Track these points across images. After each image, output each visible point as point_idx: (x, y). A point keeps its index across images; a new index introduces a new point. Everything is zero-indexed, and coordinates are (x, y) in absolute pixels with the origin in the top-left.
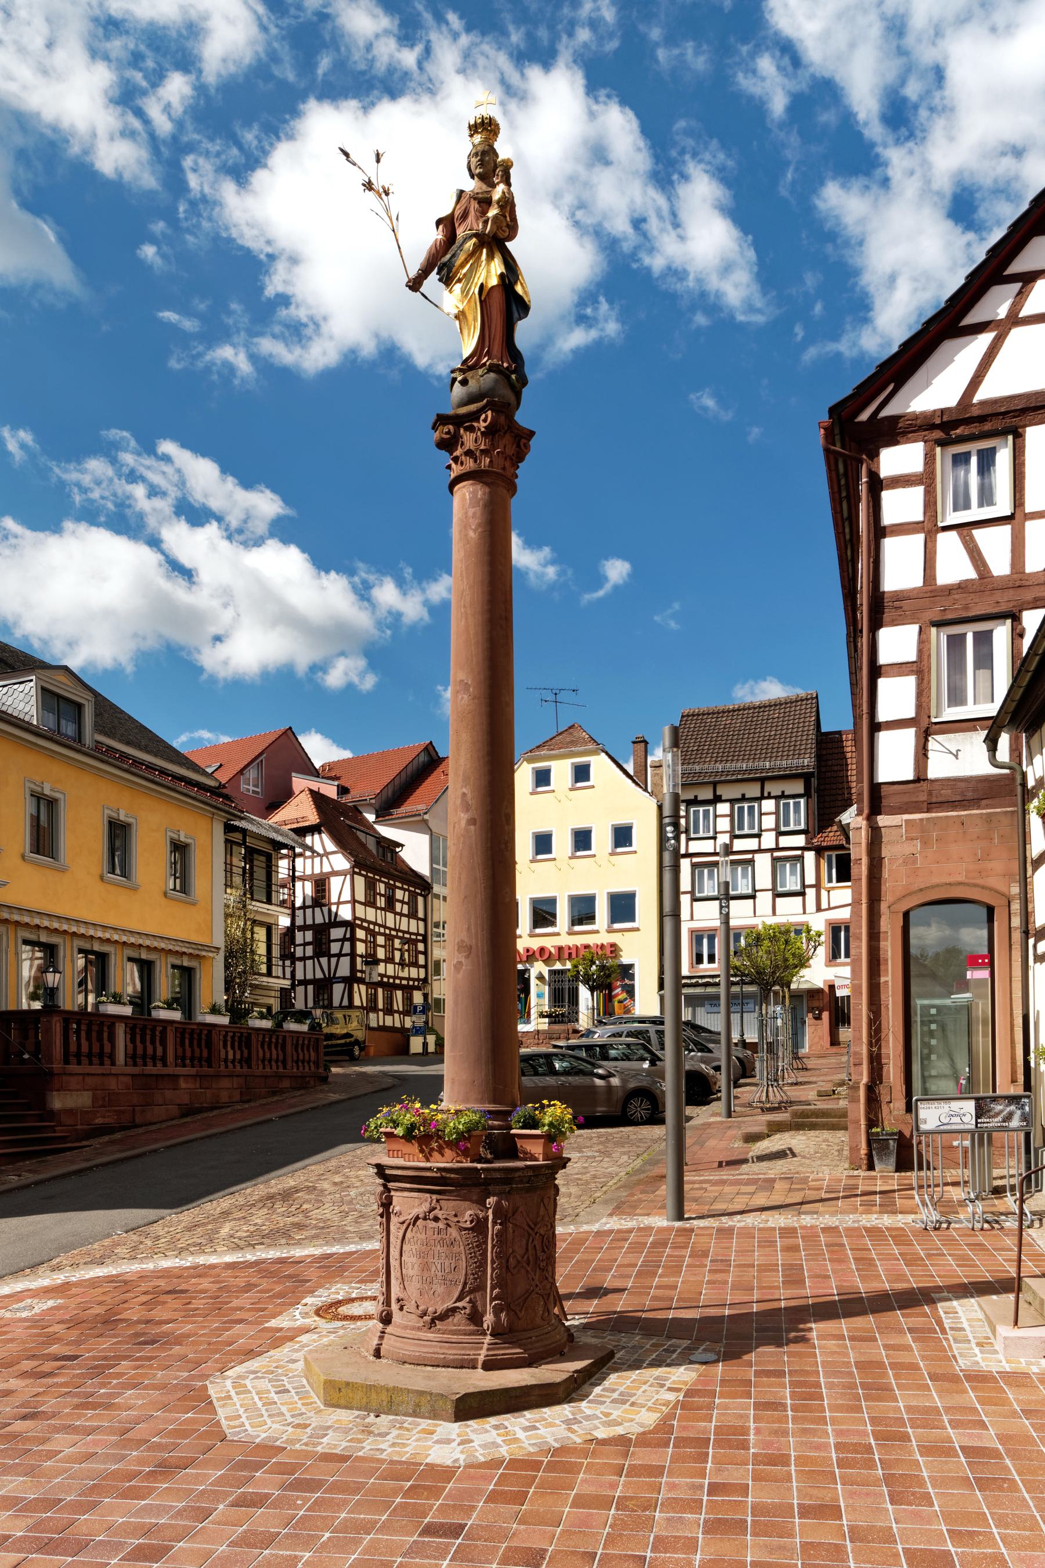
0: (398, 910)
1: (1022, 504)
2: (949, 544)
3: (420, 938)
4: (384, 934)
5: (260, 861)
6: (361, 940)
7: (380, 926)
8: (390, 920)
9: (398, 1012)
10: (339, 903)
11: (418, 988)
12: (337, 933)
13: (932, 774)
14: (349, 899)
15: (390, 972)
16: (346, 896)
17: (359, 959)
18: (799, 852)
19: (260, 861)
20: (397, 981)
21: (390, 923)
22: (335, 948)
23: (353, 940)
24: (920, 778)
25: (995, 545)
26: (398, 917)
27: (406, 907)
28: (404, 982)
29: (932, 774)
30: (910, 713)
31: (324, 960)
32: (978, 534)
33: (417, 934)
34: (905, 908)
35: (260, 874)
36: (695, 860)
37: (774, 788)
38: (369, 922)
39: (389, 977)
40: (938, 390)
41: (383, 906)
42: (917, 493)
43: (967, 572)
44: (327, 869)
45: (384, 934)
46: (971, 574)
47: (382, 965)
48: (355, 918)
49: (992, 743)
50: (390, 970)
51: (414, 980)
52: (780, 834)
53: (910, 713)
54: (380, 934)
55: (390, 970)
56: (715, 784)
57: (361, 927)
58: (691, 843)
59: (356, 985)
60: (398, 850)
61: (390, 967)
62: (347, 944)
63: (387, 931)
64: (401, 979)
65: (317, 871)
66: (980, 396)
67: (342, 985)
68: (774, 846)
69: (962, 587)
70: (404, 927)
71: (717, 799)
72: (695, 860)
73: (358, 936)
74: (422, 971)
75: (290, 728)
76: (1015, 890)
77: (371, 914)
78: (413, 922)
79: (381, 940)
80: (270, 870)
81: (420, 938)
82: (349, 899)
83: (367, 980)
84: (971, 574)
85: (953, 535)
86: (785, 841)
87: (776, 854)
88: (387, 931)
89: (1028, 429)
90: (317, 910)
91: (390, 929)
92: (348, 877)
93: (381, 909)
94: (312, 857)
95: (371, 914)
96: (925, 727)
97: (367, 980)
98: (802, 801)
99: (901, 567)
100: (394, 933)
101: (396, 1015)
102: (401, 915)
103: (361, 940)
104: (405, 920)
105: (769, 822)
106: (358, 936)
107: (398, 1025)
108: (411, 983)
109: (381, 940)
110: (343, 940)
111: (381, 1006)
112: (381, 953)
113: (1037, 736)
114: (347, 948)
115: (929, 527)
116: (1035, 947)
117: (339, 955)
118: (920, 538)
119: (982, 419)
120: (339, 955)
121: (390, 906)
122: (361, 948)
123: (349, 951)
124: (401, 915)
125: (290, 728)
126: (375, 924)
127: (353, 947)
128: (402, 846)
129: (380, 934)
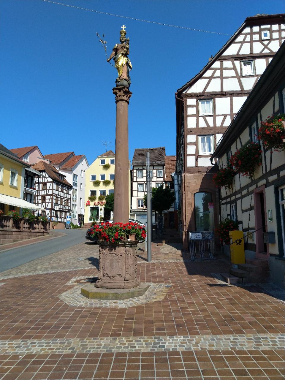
0: (64, 192)
1: (233, 112)
2: (201, 119)
3: (69, 199)
4: (60, 198)
5: (30, 178)
6: (54, 199)
7: (59, 196)
8: (62, 194)
9: (63, 218)
10: (49, 190)
11: (69, 212)
12: (48, 197)
13: (199, 165)
14: (52, 189)
15: (61, 208)
16: (51, 188)
17: (54, 204)
18: (162, 182)
19: (30, 178)
20: (63, 210)
21: (62, 195)
22: (47, 201)
23: (52, 199)
24: (196, 166)
25: (210, 120)
26: (64, 194)
27: (66, 191)
28: (65, 210)
29: (199, 165)
30: (194, 153)
31: (44, 204)
32: (207, 118)
33: (69, 198)
34: (194, 193)
35: (29, 181)
36: (138, 183)
37: (156, 168)
38: (57, 195)
39: (61, 209)
40: (198, 87)
41: (60, 191)
42: (195, 109)
43: (205, 125)
44: (46, 181)
45: (60, 198)
46: (206, 126)
47: (60, 206)
48: (53, 193)
49: (211, 160)
50: (61, 207)
51: (67, 210)
52: (158, 178)
53: (194, 153)
54: (59, 198)
55: (61, 207)
56: (143, 166)
57: (55, 196)
58: (137, 179)
59: (52, 211)
60: (64, 177)
61: (61, 206)
62: (51, 200)
63: (61, 197)
64: (64, 209)
65: (44, 181)
66: (207, 91)
67: (49, 210)
68: (156, 180)
69: (204, 128)
70: (65, 196)
71: (143, 169)
72: (138, 183)
73: (54, 198)
74: (69, 207)
75: (37, 146)
76: (217, 190)
77: (57, 193)
78: (68, 195)
79: (59, 199)
80: (32, 180)
81: (69, 199)
82: (52, 189)
83: (56, 209)
84: (206, 126)
85: (202, 118)
86: (159, 179)
87: (157, 182)
88: (61, 197)
89: (216, 99)
90: (43, 191)
91: (62, 197)
92: (52, 183)
93: (60, 192)
94: (42, 178)
95: (57, 193)
96: (197, 156)
97: (56, 209)
98: (162, 171)
99: (191, 123)
100: (63, 198)
101: (62, 219)
102: (65, 193)
103: (54, 199)
104: (66, 194)
105: (155, 175)
106: (54, 198)
107: (63, 221)
108: (67, 210)
109: (59, 199)
110: (50, 199)
111: (58, 216)
112: (59, 203)
113: (221, 159)
114: (51, 201)
115: (197, 116)
116: (222, 202)
117: (48, 203)
118: (195, 118)
119: (207, 95)
120: (48, 203)
121: (62, 192)
122: (54, 201)
123: (51, 202)
124: (65, 193)
125: (37, 146)
126: (58, 195)
127: (52, 201)
128: (66, 176)
129: (59, 198)
